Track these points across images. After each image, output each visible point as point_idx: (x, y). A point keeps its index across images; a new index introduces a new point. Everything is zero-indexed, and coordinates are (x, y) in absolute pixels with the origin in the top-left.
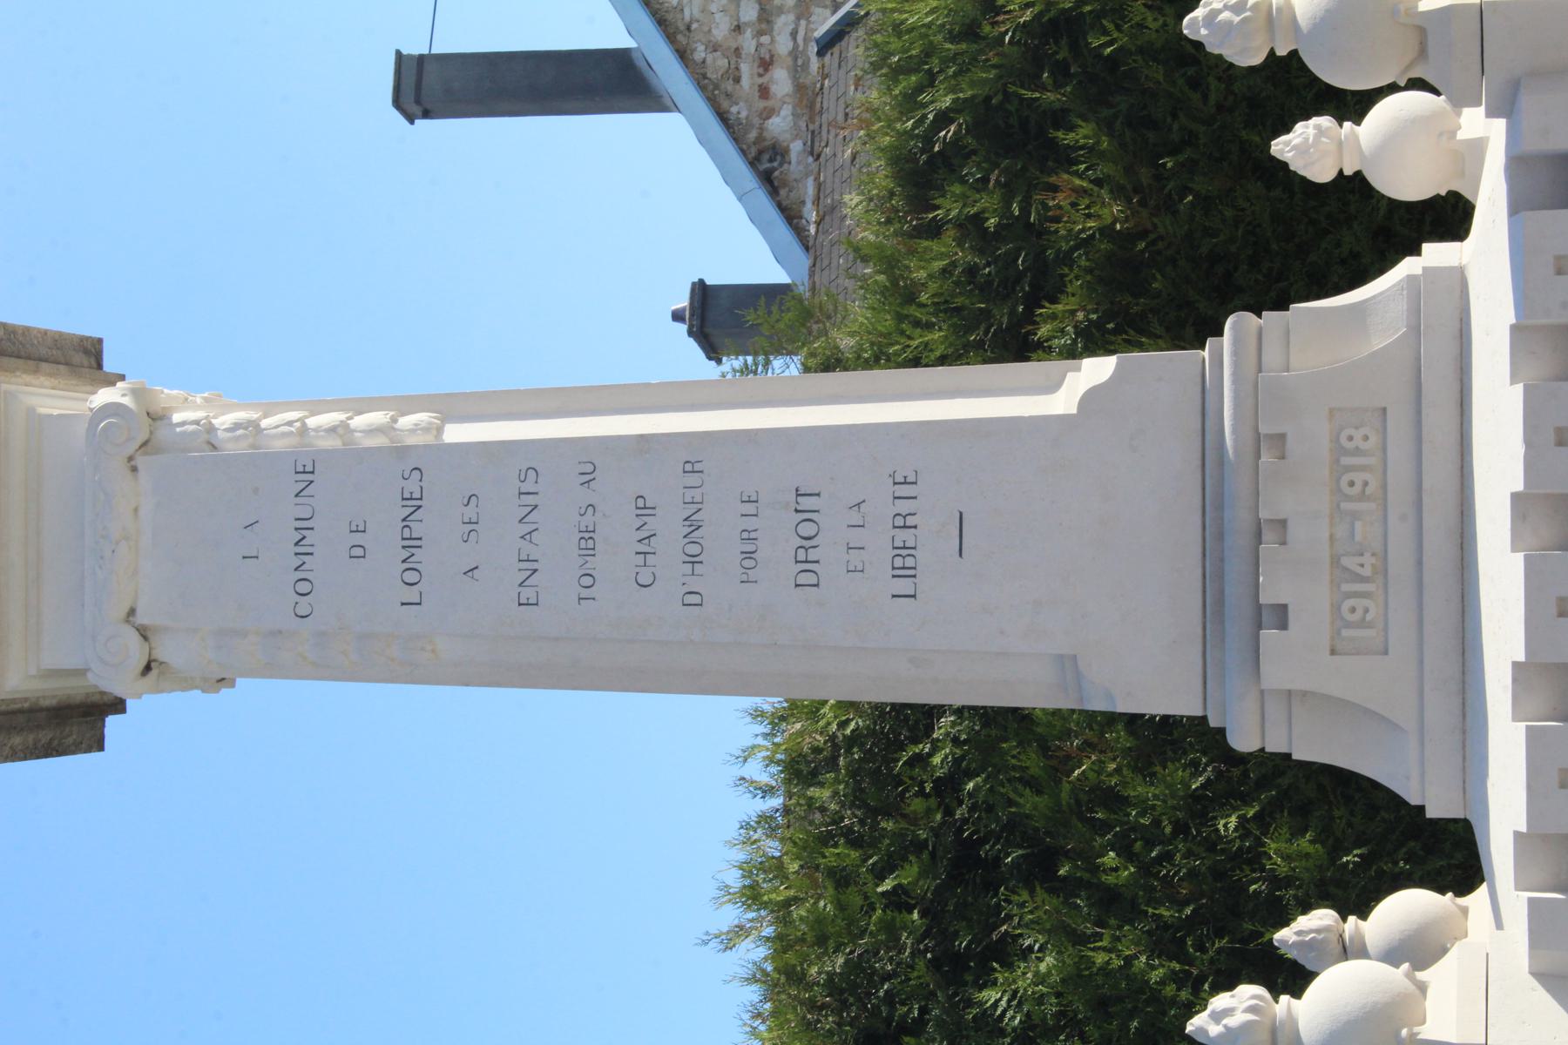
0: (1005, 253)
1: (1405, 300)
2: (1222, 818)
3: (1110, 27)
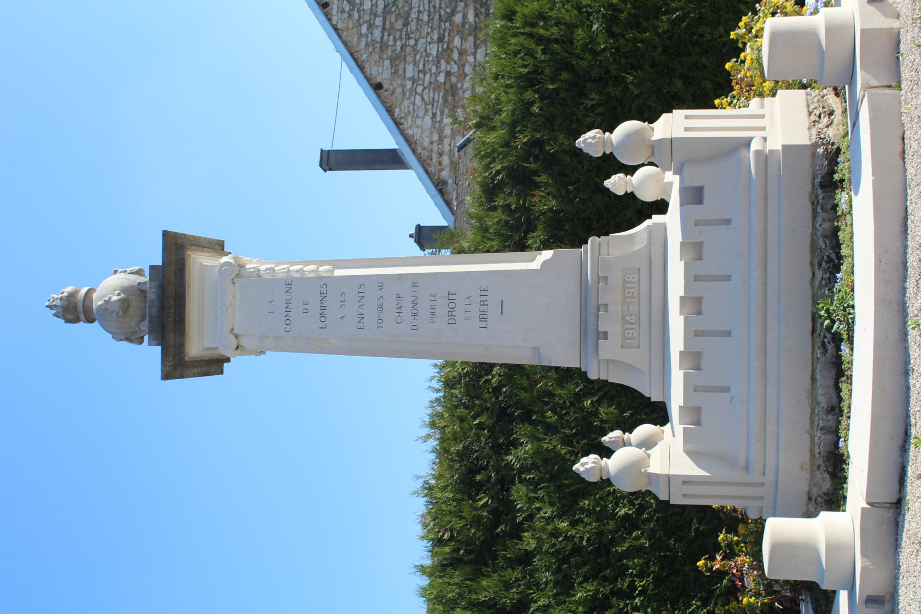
3: (552, 143)
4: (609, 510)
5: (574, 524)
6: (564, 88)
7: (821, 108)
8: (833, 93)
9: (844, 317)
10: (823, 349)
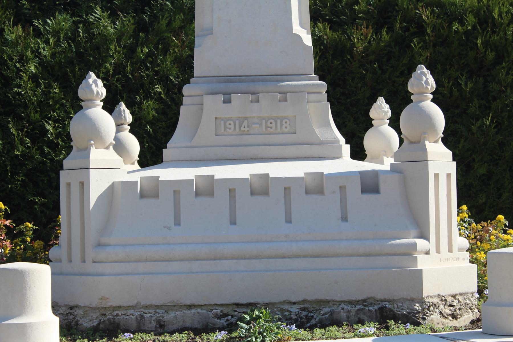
0: (346, 12)
1: (331, 139)
2: (160, 86)
3: (420, 45)
4: (50, 113)
5: (34, 78)
6: (478, 56)
7: (460, 307)
8: (475, 319)
9: (253, 333)
10: (221, 315)
